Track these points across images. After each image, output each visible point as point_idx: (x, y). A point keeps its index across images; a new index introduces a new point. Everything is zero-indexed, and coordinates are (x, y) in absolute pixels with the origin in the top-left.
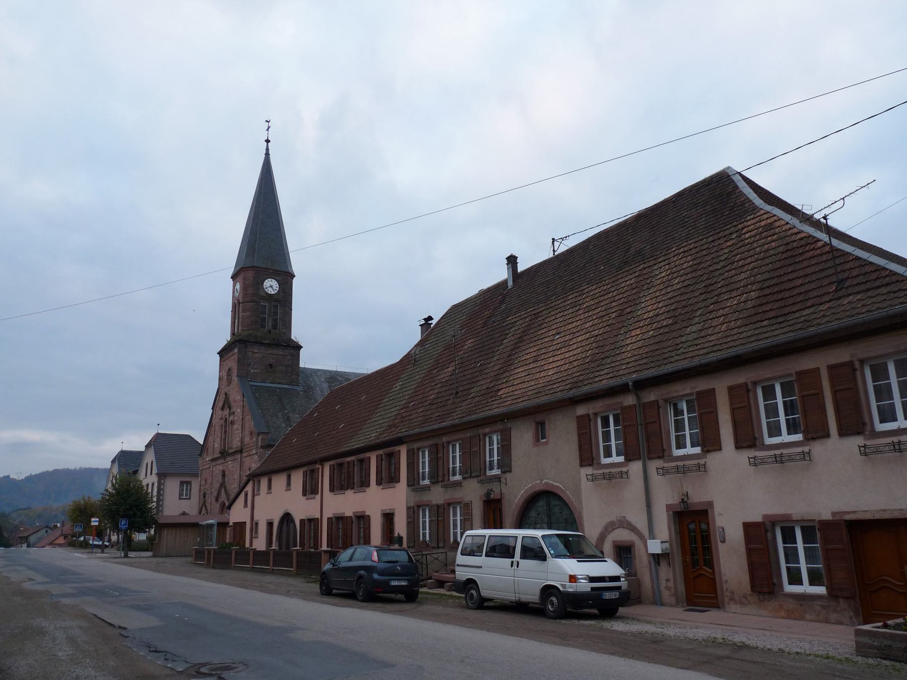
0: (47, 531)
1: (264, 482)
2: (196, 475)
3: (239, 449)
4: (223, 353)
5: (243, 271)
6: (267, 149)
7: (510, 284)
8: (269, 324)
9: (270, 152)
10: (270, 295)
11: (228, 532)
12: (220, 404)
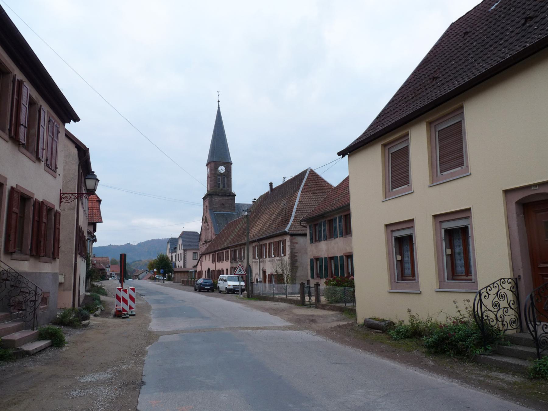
0: (147, 273)
1: (204, 257)
2: (198, 249)
3: (210, 240)
4: (204, 198)
6: (219, 105)
7: (270, 193)
8: (222, 186)
9: (220, 107)
10: (222, 173)
11: (197, 274)
12: (204, 221)
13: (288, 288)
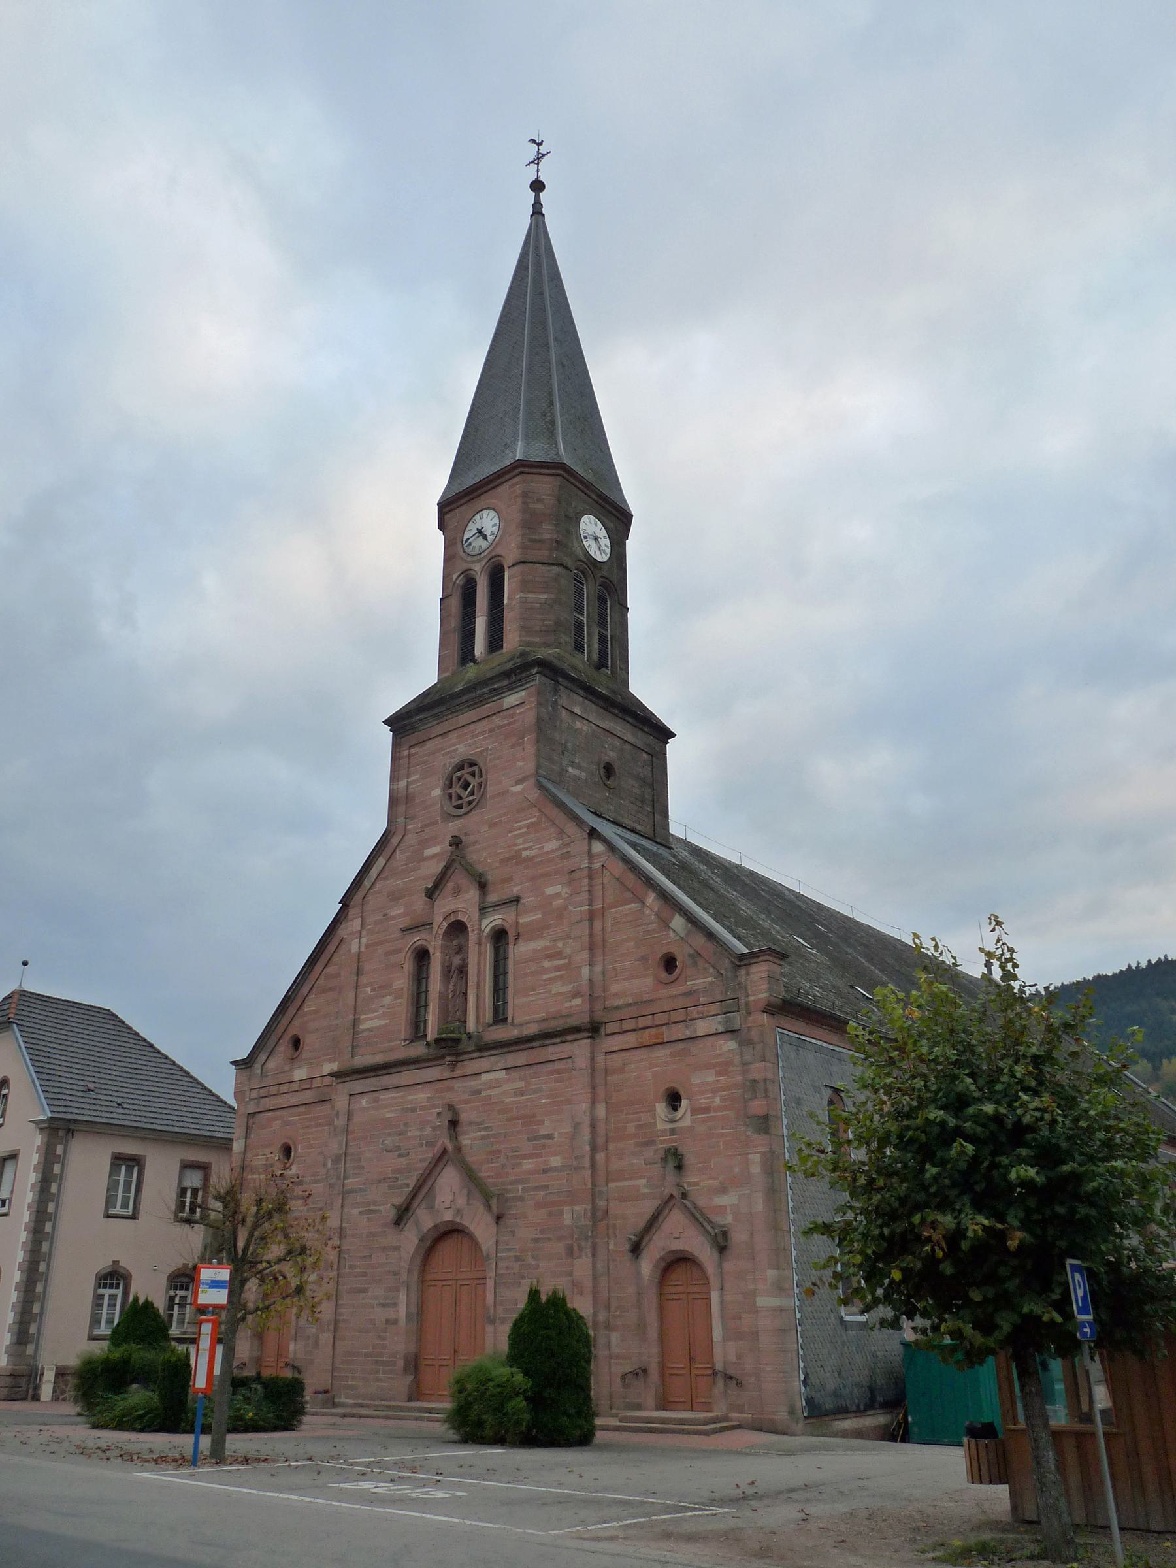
5: (521, 473)
13: (332, 1295)
